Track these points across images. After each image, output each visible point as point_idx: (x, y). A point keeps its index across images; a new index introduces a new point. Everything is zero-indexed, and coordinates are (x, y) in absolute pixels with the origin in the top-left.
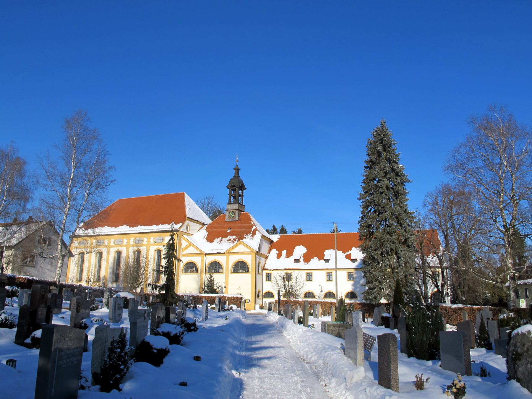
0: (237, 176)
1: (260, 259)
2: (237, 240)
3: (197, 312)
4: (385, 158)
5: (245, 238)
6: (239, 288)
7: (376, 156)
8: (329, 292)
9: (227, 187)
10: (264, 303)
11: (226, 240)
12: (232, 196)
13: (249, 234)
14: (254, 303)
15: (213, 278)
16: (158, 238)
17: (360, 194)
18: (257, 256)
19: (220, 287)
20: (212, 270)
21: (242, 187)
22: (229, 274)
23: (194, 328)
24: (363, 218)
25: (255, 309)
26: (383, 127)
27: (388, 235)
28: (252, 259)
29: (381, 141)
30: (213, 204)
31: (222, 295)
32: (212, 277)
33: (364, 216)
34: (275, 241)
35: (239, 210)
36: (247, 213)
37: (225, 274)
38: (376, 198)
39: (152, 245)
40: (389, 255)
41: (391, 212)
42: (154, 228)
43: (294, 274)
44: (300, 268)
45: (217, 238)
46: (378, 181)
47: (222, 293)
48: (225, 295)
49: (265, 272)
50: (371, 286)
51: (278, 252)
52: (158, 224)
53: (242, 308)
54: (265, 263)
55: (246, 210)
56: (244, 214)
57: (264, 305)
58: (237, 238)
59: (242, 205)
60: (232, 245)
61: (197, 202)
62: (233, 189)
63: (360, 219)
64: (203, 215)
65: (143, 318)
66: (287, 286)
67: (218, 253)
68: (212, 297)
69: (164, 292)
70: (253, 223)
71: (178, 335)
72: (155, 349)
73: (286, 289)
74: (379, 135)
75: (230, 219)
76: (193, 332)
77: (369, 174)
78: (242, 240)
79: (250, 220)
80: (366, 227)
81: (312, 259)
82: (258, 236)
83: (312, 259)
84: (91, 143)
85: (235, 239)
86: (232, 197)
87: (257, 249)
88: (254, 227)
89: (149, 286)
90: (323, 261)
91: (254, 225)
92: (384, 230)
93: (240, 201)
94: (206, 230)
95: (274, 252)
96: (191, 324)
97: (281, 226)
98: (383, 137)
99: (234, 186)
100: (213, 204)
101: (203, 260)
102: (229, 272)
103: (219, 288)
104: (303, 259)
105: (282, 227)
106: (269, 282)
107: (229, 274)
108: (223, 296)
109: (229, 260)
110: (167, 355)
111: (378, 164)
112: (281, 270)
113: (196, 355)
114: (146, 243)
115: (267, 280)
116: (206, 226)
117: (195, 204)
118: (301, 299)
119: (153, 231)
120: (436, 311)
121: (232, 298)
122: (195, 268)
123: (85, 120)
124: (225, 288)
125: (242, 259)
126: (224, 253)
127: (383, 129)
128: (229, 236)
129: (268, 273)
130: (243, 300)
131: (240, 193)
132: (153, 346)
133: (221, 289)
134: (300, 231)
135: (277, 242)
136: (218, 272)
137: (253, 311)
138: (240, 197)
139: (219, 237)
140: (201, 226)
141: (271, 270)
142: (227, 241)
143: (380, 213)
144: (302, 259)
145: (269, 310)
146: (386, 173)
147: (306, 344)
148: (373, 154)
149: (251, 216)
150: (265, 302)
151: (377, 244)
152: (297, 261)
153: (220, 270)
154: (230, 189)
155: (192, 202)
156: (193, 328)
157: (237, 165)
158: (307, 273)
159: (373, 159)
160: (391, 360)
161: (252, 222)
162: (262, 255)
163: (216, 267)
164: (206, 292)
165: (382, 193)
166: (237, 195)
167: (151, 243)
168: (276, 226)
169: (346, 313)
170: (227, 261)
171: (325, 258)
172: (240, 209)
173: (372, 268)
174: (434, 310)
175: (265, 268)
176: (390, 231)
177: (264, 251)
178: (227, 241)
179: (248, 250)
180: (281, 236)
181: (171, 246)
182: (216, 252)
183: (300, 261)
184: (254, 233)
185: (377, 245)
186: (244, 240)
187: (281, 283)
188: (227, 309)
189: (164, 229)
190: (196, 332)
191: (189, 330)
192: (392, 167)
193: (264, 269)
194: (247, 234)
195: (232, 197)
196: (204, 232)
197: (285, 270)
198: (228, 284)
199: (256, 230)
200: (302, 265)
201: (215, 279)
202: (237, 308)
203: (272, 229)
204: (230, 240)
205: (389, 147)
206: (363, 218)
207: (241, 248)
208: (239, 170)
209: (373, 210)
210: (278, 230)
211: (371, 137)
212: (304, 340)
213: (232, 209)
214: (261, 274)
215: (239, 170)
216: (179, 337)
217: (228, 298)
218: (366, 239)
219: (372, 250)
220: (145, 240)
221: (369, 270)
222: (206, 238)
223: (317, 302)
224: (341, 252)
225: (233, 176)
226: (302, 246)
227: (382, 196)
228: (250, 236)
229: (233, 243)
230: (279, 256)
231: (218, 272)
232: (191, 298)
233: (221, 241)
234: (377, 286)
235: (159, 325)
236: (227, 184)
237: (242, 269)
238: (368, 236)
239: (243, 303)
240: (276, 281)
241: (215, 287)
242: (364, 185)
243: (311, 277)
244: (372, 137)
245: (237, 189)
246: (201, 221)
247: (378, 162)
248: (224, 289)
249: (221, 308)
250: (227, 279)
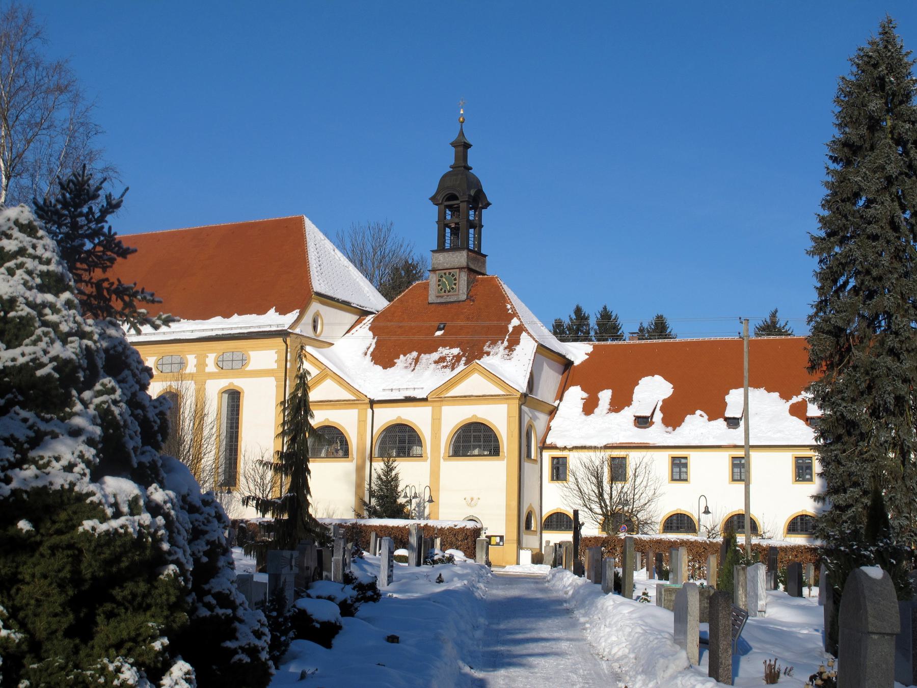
0: (461, 167)
1: (534, 418)
2: (464, 359)
3: (365, 566)
4: (891, 132)
5: (488, 354)
6: (471, 502)
7: (864, 131)
8: (802, 516)
9: (433, 199)
10: (544, 544)
11: (431, 361)
12: (447, 226)
13: (500, 342)
14: (515, 546)
15: (393, 473)
16: (228, 356)
17: (814, 239)
18: (523, 407)
19: (417, 500)
20: (392, 448)
21: (478, 201)
22: (442, 460)
23: (372, 594)
24: (821, 309)
25: (518, 563)
26: (887, 41)
27: (889, 359)
28: (509, 417)
29: (880, 85)
30: (388, 247)
31: (422, 523)
32: (391, 470)
33: (826, 301)
34: (577, 362)
35: (470, 270)
36: (492, 279)
37: (429, 460)
38: (857, 254)
39: (211, 376)
40: (894, 415)
41: (902, 293)
42: (216, 325)
43: (634, 458)
44: (652, 442)
45: (405, 355)
46: (869, 203)
47: (421, 516)
48: (431, 523)
49: (547, 455)
50: (841, 499)
51: (585, 395)
52: (227, 315)
53: (481, 558)
54: (549, 429)
55: (491, 269)
56: (483, 280)
57: (543, 552)
58: (464, 355)
59: (478, 255)
60: (449, 374)
61: (342, 241)
62: (450, 207)
63: (812, 311)
64: (362, 284)
65: (289, 567)
66: (606, 497)
67: (409, 400)
68: (393, 528)
69: (286, 517)
70: (513, 308)
71: (349, 602)
72: (317, 622)
73: (606, 506)
74: (875, 66)
75: (442, 297)
76: (371, 603)
77: (842, 182)
78: (479, 359)
79: (504, 299)
80: (829, 332)
81: (688, 418)
82: (526, 347)
83: (688, 416)
84: (51, 104)
85: (458, 358)
86: (448, 230)
87: (523, 387)
88: (515, 322)
89: (250, 502)
90: (721, 423)
91: (515, 315)
92: (882, 343)
93: (471, 242)
94: (370, 329)
95: (575, 395)
96: (367, 585)
97: (601, 309)
98: (886, 72)
99: (452, 197)
100: (388, 247)
101: (365, 421)
102: (442, 455)
103: (414, 501)
104: (662, 415)
105: (606, 316)
106: (557, 485)
107: (442, 460)
108: (426, 525)
109: (440, 419)
110: (337, 633)
111: (870, 153)
112: (595, 448)
113: (390, 634)
114: (194, 370)
115: (552, 479)
116: (370, 318)
117: (337, 251)
118: (655, 533)
119: (213, 333)
120: (895, 562)
121: (451, 530)
122: (341, 442)
123: (28, 37)
124: (431, 501)
125: (480, 415)
126: (425, 400)
127: (886, 47)
128: (440, 349)
129: (558, 458)
130: (483, 537)
131: (471, 218)
132: (314, 617)
133: (418, 505)
134: (660, 328)
135: (584, 363)
136: (409, 456)
137: (512, 569)
138: (471, 231)
139: (410, 352)
140: (356, 318)
141: (565, 448)
142: (436, 362)
143: (870, 296)
144: (658, 416)
145: (554, 565)
146: (890, 180)
147: (615, 629)
148: (855, 123)
149: (505, 286)
150: (548, 542)
151: (858, 383)
152: (643, 422)
153: (416, 450)
154: (442, 207)
155: (328, 245)
156: (370, 593)
157: (462, 133)
158: (674, 458)
159: (854, 139)
160: (721, 634)
161: (509, 306)
162: (539, 405)
163: (402, 441)
164: (374, 513)
165: (875, 238)
166: (463, 224)
167: (208, 370)
168: (588, 310)
169: (735, 569)
170: (436, 421)
171: (728, 414)
172: (472, 266)
173: (844, 451)
174: (892, 561)
175: (548, 441)
176: (897, 345)
177: (546, 391)
178: (436, 362)
179: (496, 391)
180: (595, 347)
181: (300, 402)
182: (400, 396)
183: (652, 423)
184: (514, 342)
185: (857, 387)
186: (485, 361)
187: (590, 488)
188: (439, 559)
189: (246, 328)
190: (377, 603)
191: (367, 600)
192: (911, 160)
193: (544, 447)
194: (494, 343)
195: (448, 230)
196: (364, 337)
197: (606, 447)
198: (438, 490)
199: (519, 330)
200: (657, 433)
201: (400, 477)
202: (465, 558)
203: (574, 317)
204: (442, 359)
205: (901, 103)
206: (821, 306)
207: (475, 384)
208: (467, 146)
209: (852, 283)
210: (593, 322)
211: (849, 72)
212: (613, 622)
213: (448, 266)
214: (535, 461)
215: (467, 146)
216: (352, 605)
217: (442, 529)
218: (831, 367)
219: (843, 399)
220: (192, 361)
221: (836, 456)
222: (372, 354)
223: (692, 543)
224: (777, 394)
225: (451, 167)
226: (658, 378)
227: (875, 247)
228: (502, 348)
229: (453, 369)
230: (589, 407)
231: (409, 453)
232: (342, 531)
233: (416, 364)
234: (857, 500)
235: (310, 584)
236: (433, 191)
237: (480, 447)
238: (837, 358)
239: (483, 544)
240: (577, 482)
241: (402, 500)
242: (826, 213)
243: (684, 470)
244: (852, 73)
245: (463, 206)
246: (355, 301)
247: (867, 145)
248: (427, 504)
249: (424, 555)
250: (435, 474)
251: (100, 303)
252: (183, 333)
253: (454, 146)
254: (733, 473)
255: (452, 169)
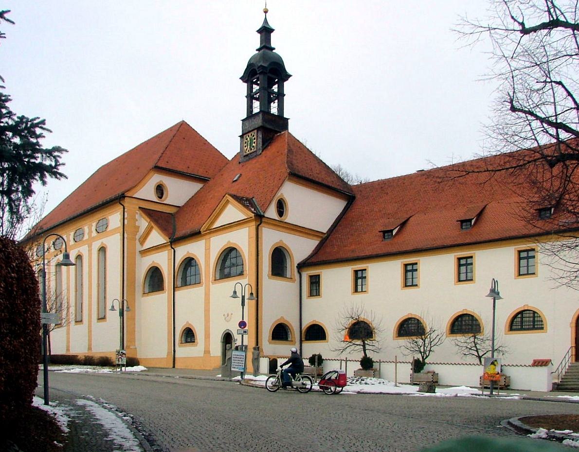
157: (266, 21)
170: (208, 249)
251: (14, 187)
252: (290, 269)
253: (259, 33)
254: (459, 273)
255: (258, 52)
